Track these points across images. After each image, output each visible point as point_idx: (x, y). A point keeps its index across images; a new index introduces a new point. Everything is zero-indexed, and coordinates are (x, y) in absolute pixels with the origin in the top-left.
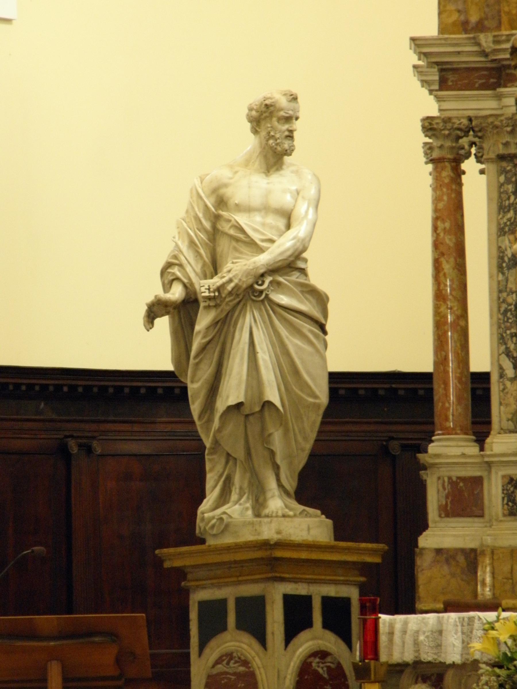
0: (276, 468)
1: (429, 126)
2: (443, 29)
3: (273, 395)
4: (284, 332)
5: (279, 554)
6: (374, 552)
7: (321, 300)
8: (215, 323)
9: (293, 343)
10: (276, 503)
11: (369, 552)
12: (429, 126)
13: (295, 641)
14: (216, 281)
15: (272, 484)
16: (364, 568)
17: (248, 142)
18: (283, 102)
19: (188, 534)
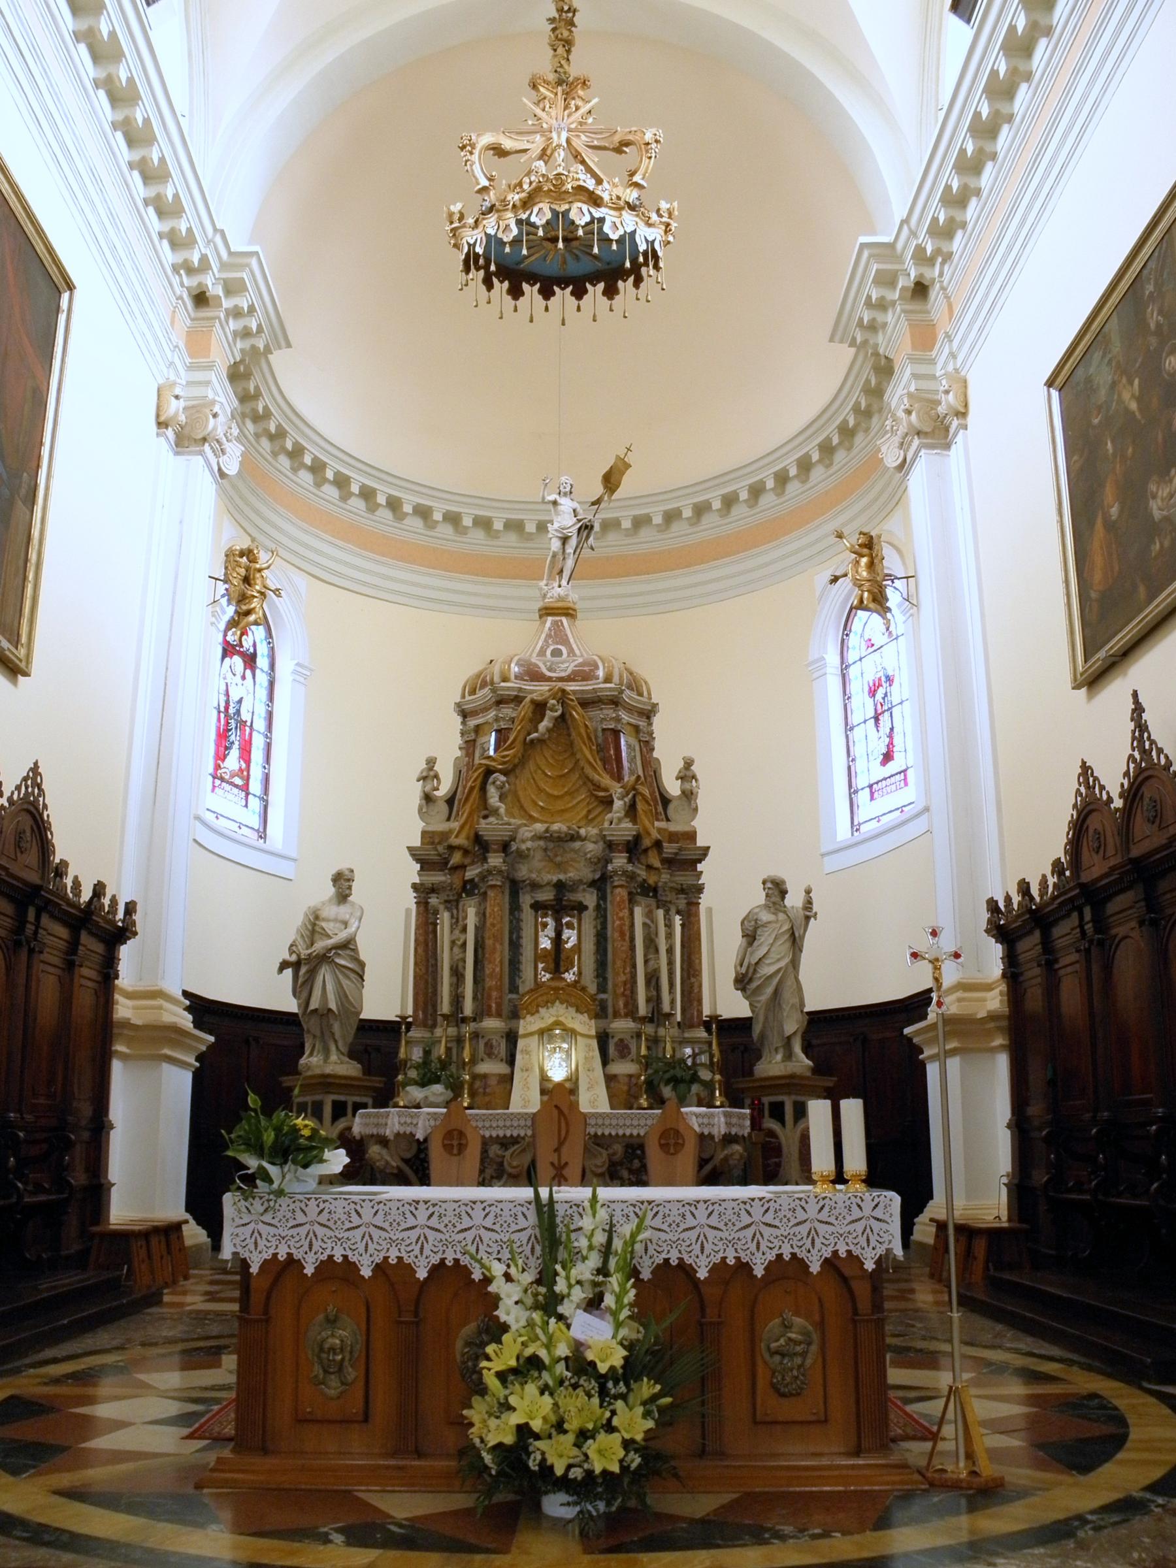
0: (336, 1042)
1: (415, 887)
2: (422, 843)
3: (333, 1005)
4: (341, 977)
5: (329, 1080)
6: (380, 1082)
7: (362, 965)
8: (307, 972)
9: (345, 982)
10: (334, 1057)
11: (377, 1081)
12: (415, 887)
13: (336, 1123)
14: (309, 951)
15: (333, 1048)
16: (375, 1089)
17: (331, 890)
18: (347, 873)
19: (294, 1071)
